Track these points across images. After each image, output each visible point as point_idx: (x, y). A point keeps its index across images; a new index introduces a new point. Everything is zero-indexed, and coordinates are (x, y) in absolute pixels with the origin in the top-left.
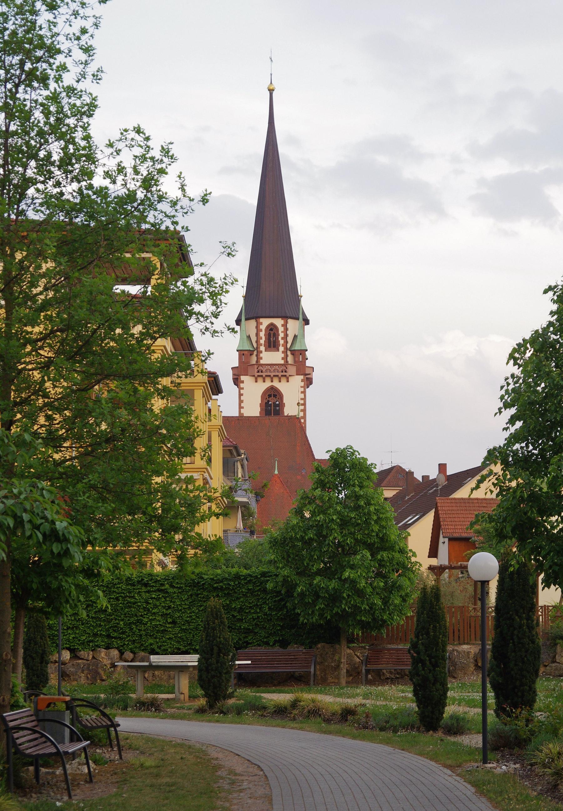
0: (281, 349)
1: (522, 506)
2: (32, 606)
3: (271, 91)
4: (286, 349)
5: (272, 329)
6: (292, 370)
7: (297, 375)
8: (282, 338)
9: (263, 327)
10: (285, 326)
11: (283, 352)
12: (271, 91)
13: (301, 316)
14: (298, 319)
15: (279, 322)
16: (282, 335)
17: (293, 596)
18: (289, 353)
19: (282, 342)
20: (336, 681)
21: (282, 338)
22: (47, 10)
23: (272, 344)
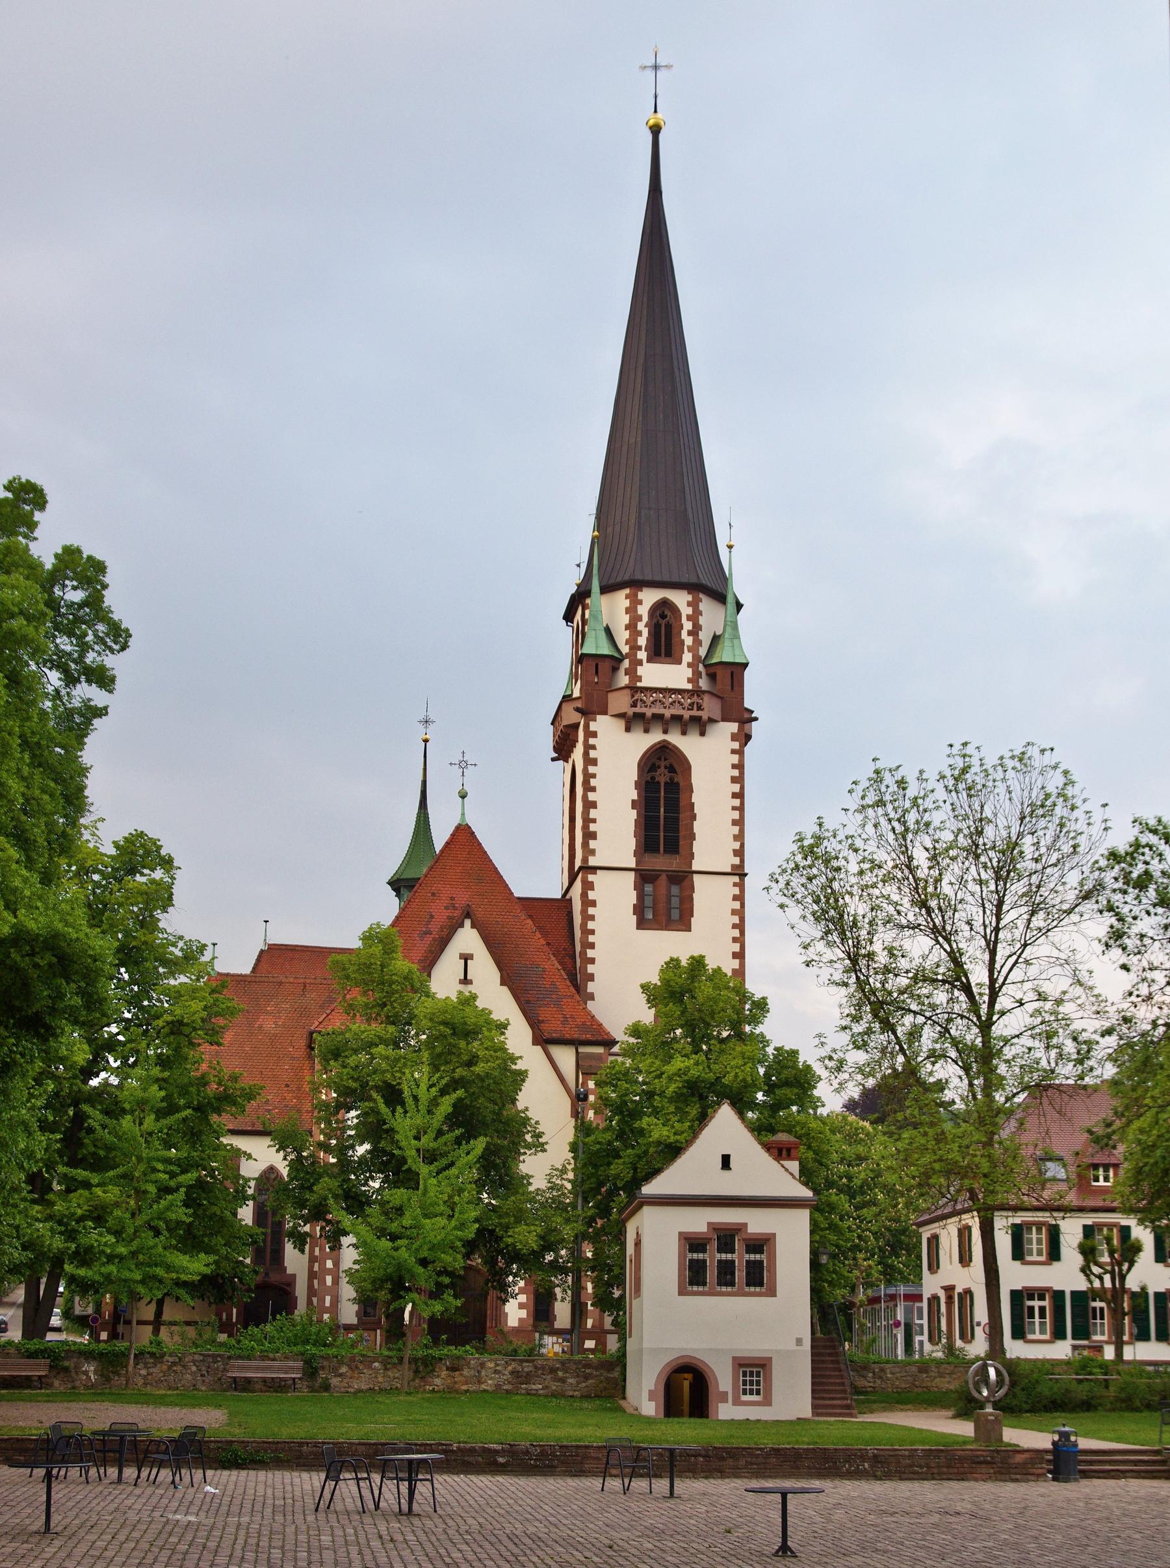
0: (687, 657)
3: (656, 130)
4: (696, 657)
5: (663, 610)
6: (711, 707)
8: (690, 633)
9: (643, 611)
10: (694, 604)
11: (689, 665)
12: (656, 130)
15: (681, 599)
16: (688, 626)
18: (701, 668)
23: (664, 646)
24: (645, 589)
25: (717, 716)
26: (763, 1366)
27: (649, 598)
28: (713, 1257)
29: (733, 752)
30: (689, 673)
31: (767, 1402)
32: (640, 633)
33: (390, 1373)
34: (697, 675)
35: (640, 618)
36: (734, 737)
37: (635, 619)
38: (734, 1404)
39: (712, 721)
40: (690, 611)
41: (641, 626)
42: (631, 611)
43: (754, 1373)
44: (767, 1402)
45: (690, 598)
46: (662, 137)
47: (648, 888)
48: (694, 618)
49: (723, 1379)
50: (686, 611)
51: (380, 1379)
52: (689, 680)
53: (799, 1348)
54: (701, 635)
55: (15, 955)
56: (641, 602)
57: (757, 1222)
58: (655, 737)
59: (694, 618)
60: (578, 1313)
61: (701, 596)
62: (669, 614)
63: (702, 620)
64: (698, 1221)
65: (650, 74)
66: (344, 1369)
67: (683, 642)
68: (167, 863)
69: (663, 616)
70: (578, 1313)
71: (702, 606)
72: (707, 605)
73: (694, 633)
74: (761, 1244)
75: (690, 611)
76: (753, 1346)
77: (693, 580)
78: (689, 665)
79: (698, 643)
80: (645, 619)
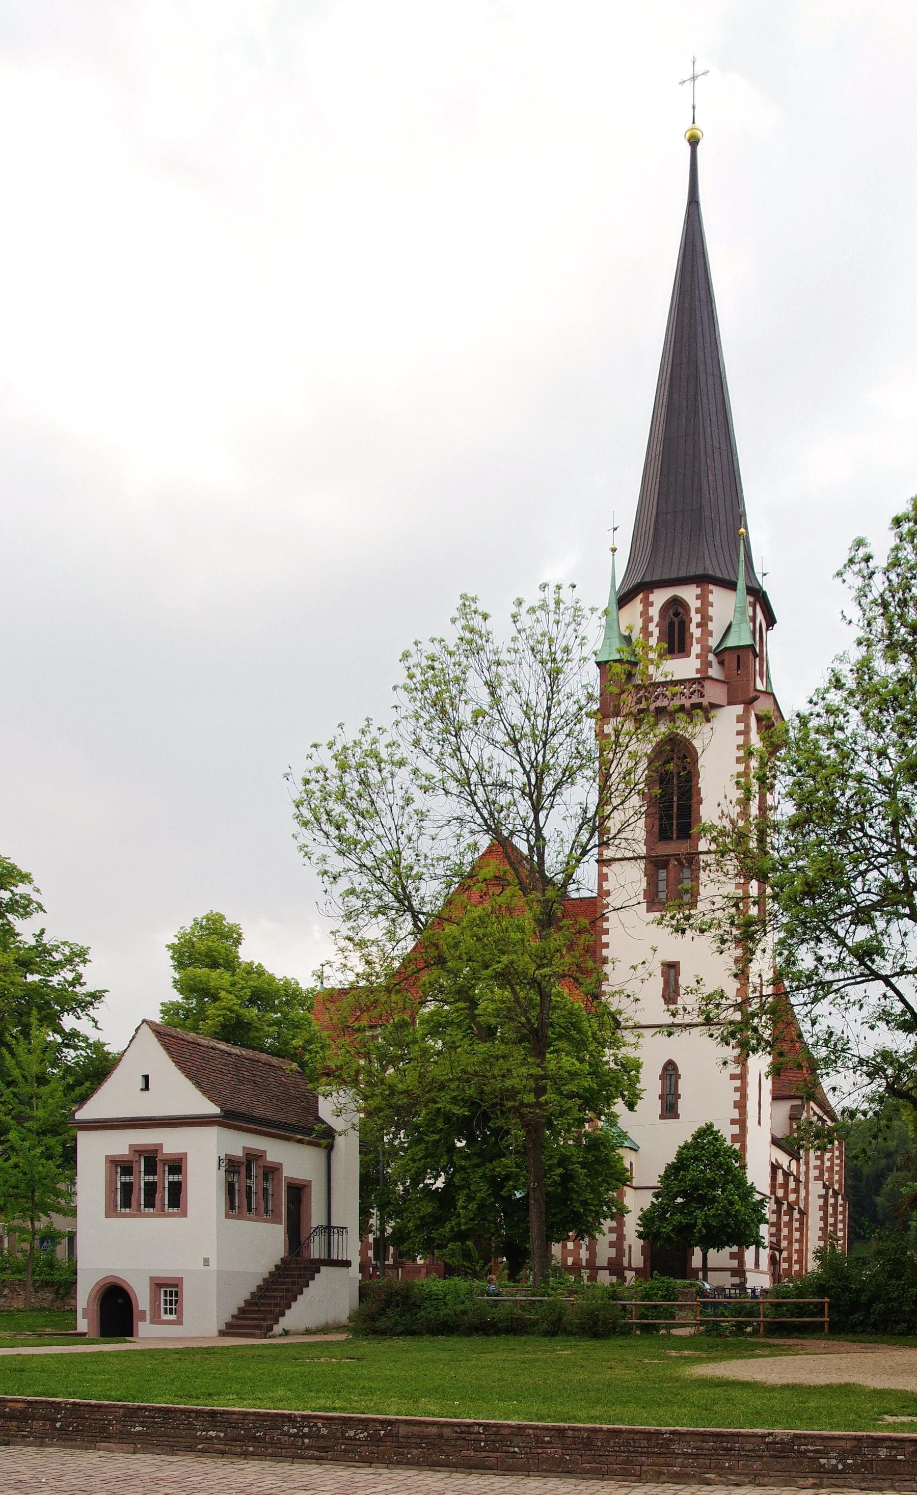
0: (696, 649)
1: (440, 1183)
2: (378, 1233)
3: (694, 142)
4: (706, 649)
5: (676, 608)
6: (714, 693)
7: (730, 703)
8: (698, 625)
9: (654, 612)
10: (703, 597)
11: (698, 656)
12: (694, 142)
13: (741, 585)
14: (731, 586)
15: (689, 594)
16: (696, 618)
17: (758, 779)
18: (711, 657)
19: (696, 632)
20: (662, 896)
21: (698, 625)
22: (718, 1251)
23: (676, 640)
24: (655, 591)
25: (725, 702)
26: (176, 1286)
27: (659, 598)
28: (142, 1179)
29: (739, 733)
30: (697, 664)
31: (179, 1322)
32: (651, 634)
33: (39, 1295)
34: (707, 664)
35: (651, 619)
36: (739, 719)
37: (647, 620)
38: (152, 1322)
39: (714, 706)
40: (698, 604)
41: (652, 627)
42: (645, 615)
43: (169, 1291)
44: (179, 1322)
45: (698, 591)
46: (699, 148)
47: (663, 874)
48: (703, 611)
49: (143, 1300)
50: (694, 604)
51: (33, 1300)
52: (698, 671)
53: (206, 1268)
54: (711, 626)
55: (767, 1034)
56: (652, 604)
57: (171, 1142)
58: (663, 729)
59: (703, 611)
60: (381, 1248)
61: (711, 587)
62: (681, 611)
63: (711, 611)
64: (120, 1143)
65: (689, 85)
66: (6, 1292)
67: (692, 635)
68: (25, 878)
69: (676, 614)
70: (381, 1248)
71: (711, 598)
72: (717, 595)
73: (702, 625)
74: (177, 1166)
75: (698, 604)
76: (167, 1268)
77: (700, 572)
78: (698, 656)
79: (707, 633)
80: (656, 619)
